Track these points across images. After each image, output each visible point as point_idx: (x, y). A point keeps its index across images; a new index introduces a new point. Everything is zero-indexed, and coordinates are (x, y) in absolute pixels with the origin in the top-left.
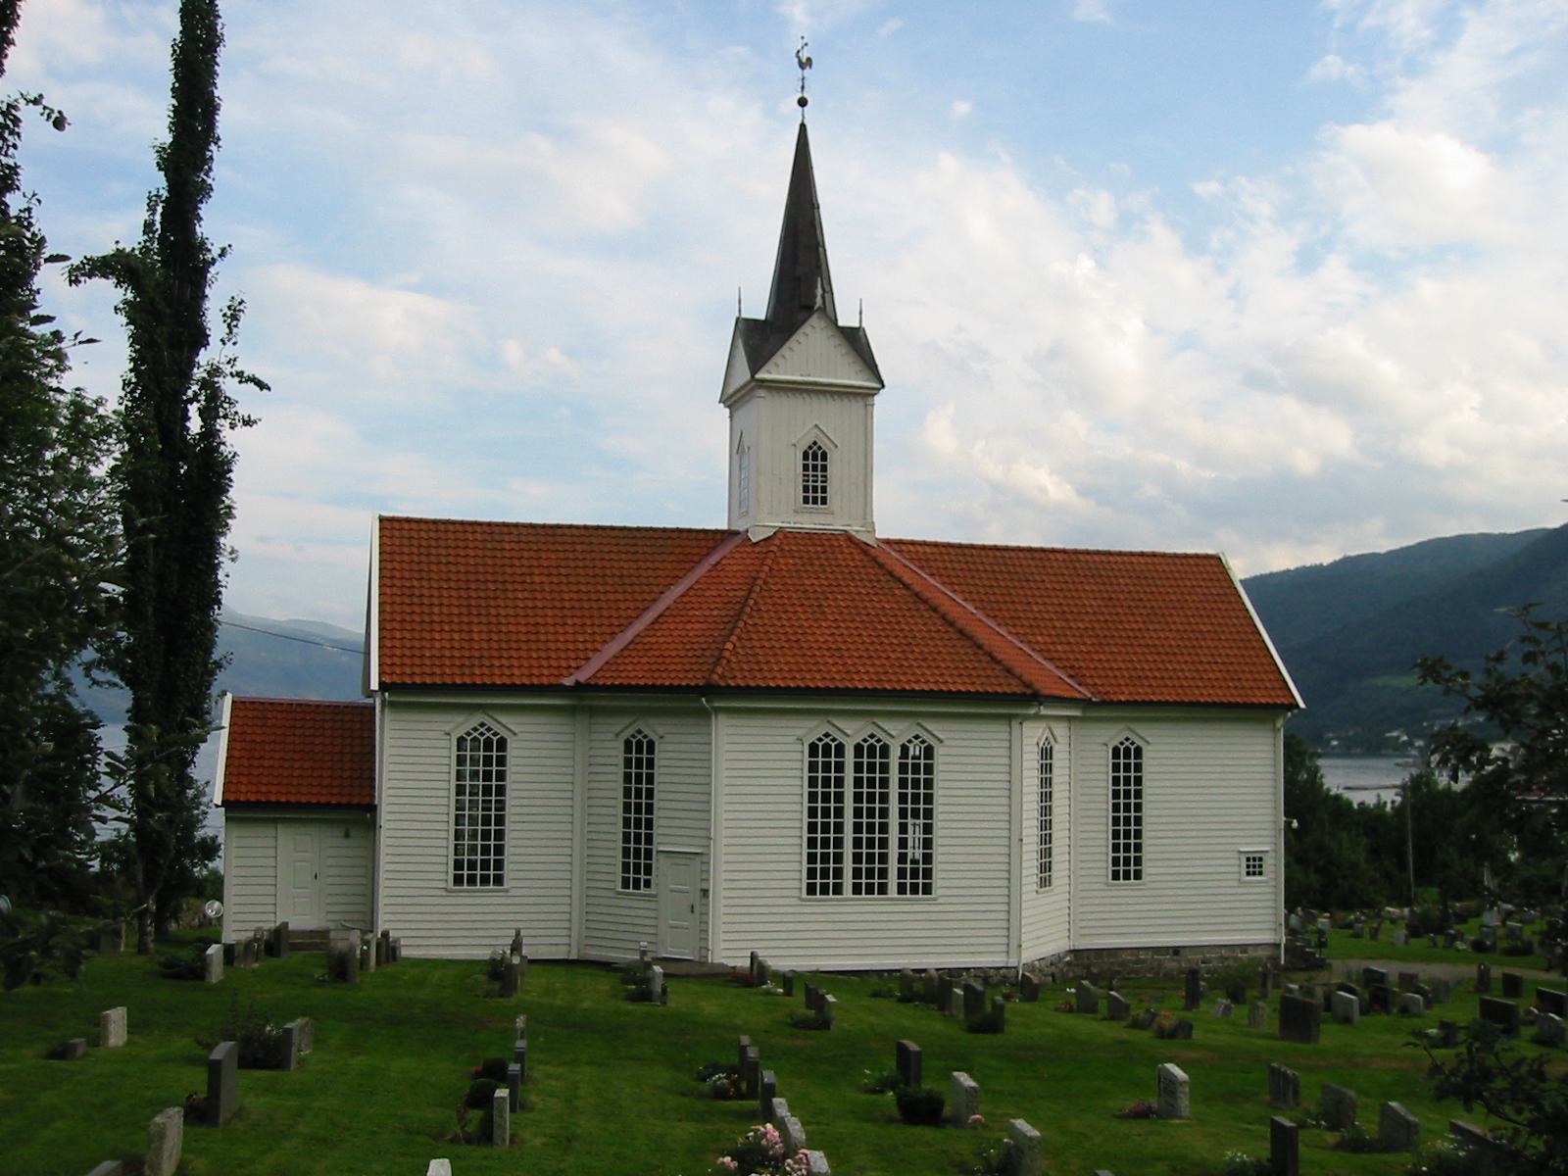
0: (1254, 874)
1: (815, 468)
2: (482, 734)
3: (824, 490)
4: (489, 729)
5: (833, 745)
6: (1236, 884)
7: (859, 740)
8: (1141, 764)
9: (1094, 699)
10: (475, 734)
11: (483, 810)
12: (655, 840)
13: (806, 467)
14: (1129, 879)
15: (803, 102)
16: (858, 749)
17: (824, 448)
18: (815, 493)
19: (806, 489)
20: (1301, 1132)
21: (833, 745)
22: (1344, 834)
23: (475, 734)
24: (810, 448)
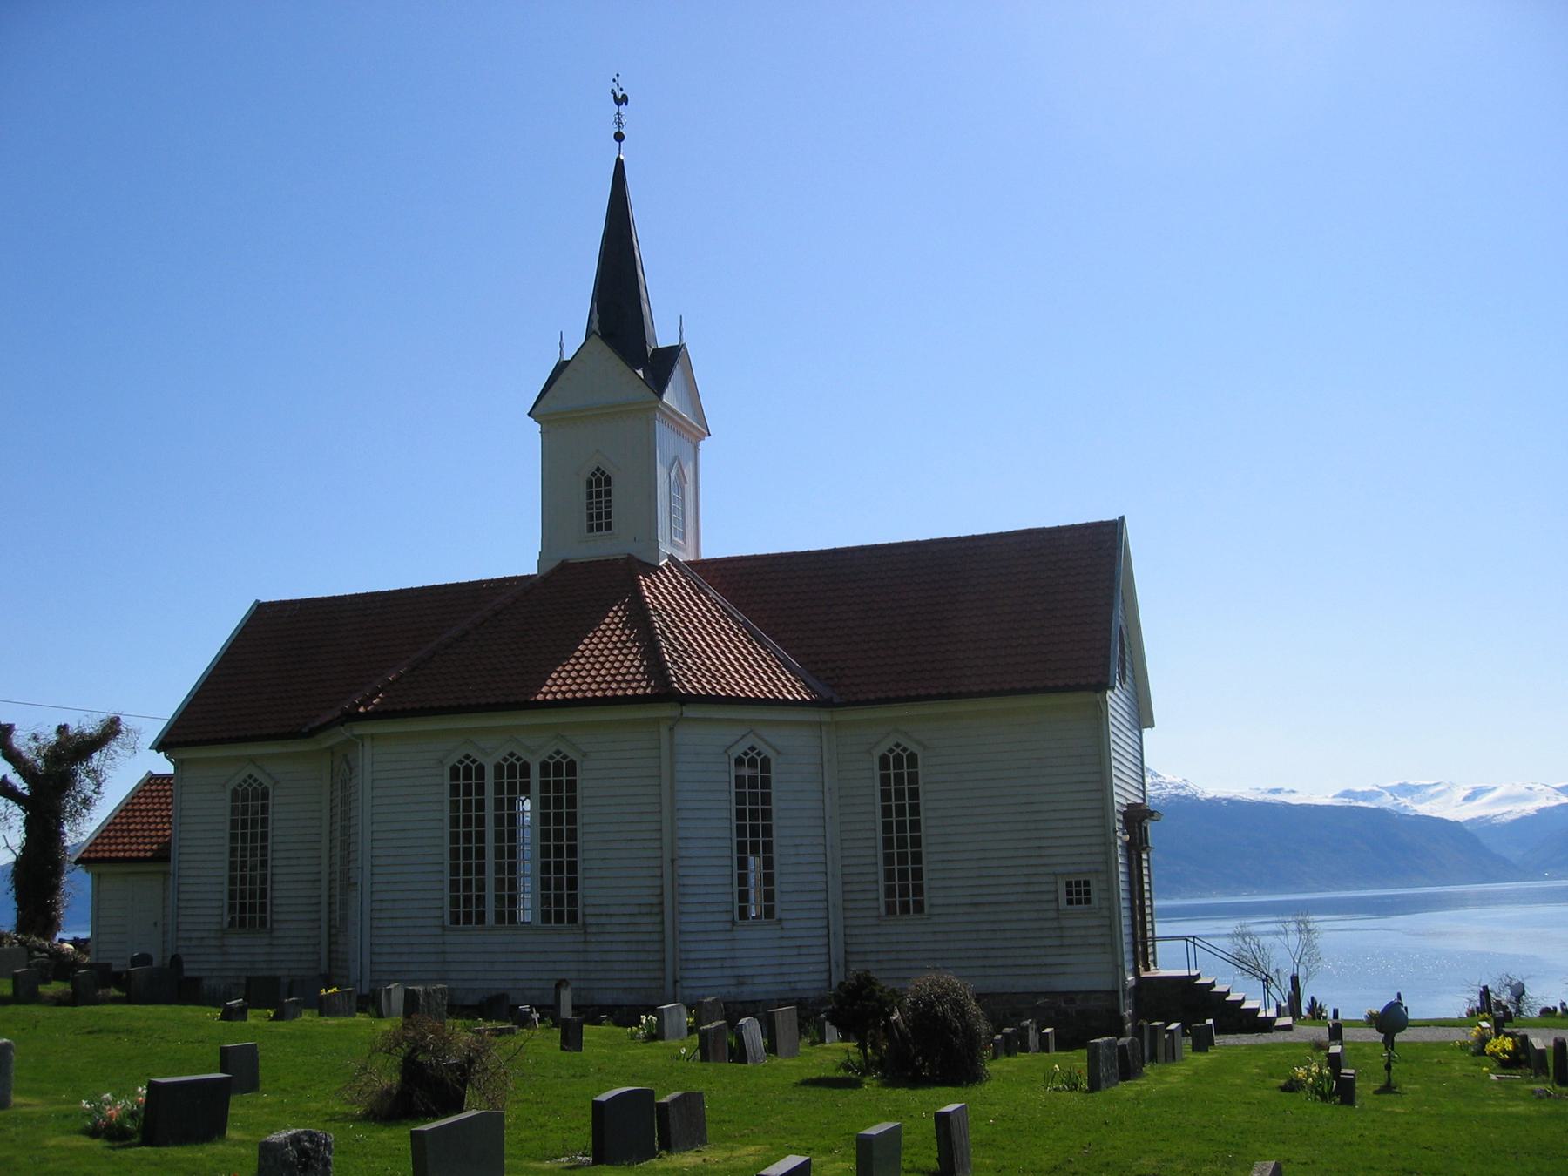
0: (1069, 893)
1: (599, 494)
2: (250, 785)
3: (608, 515)
4: (255, 780)
5: (518, 764)
6: (439, 931)
7: (544, 757)
8: (610, 490)
9: (1432, 1112)
10: (245, 786)
11: (241, 857)
12: (227, 865)
13: (590, 496)
14: (471, 923)
15: (619, 137)
16: (544, 767)
17: (607, 472)
18: (600, 520)
19: (590, 517)
20: (1278, 1019)
21: (518, 764)
22: (920, 1138)
23: (245, 786)
24: (594, 474)
